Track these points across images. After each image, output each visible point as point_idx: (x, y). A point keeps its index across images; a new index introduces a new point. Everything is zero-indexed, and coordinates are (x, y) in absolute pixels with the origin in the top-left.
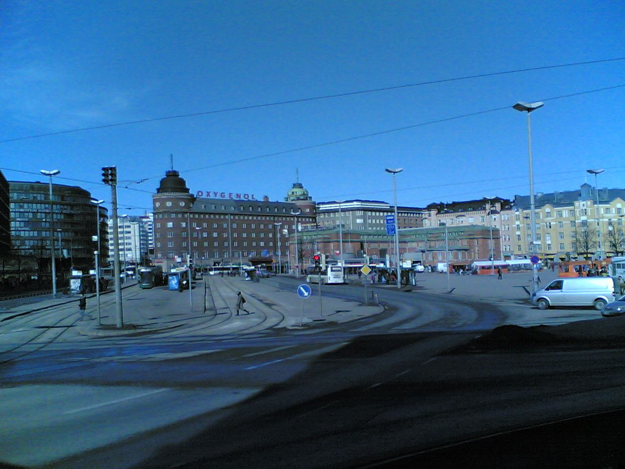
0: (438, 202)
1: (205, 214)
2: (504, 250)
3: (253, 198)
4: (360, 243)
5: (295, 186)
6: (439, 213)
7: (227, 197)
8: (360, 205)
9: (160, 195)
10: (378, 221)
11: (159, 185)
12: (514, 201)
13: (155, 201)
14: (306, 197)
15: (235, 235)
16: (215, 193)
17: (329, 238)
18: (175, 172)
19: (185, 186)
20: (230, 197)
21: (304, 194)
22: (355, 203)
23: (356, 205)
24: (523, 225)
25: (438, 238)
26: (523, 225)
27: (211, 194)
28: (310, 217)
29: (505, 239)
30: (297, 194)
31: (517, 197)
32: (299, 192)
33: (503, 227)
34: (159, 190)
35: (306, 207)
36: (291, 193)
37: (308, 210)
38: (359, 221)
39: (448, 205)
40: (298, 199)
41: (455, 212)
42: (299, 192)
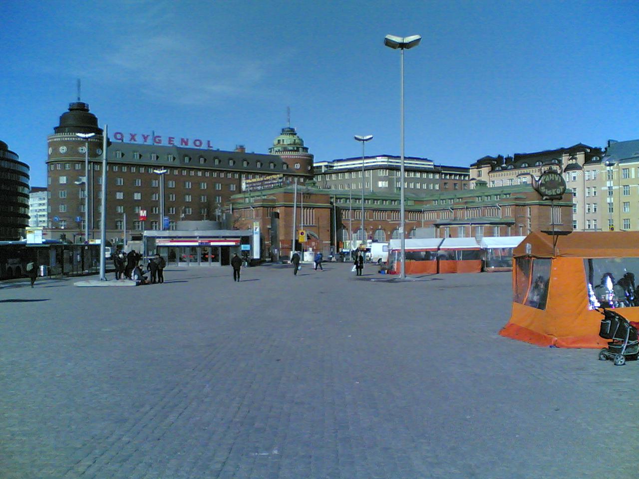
0: (494, 155)
1: (138, 166)
2: (587, 228)
3: (209, 146)
4: (330, 210)
5: (284, 132)
6: (493, 170)
7: (165, 142)
8: (388, 162)
9: (59, 135)
10: (412, 185)
11: (58, 122)
12: (605, 152)
13: (54, 145)
14: (298, 146)
15: (173, 198)
16: (143, 135)
17: (274, 201)
18: (84, 104)
19: (97, 125)
20: (170, 143)
21: (294, 143)
22: (379, 159)
23: (380, 161)
24: (617, 187)
25: (469, 205)
26: (617, 187)
27: (136, 137)
28: (302, 176)
29: (589, 209)
30: (285, 143)
31: (611, 143)
32: (287, 139)
33: (587, 190)
34: (58, 130)
35: (296, 161)
36: (277, 141)
37: (298, 166)
38: (381, 184)
39: (508, 159)
40: (285, 150)
41: (515, 168)
42: (287, 139)
